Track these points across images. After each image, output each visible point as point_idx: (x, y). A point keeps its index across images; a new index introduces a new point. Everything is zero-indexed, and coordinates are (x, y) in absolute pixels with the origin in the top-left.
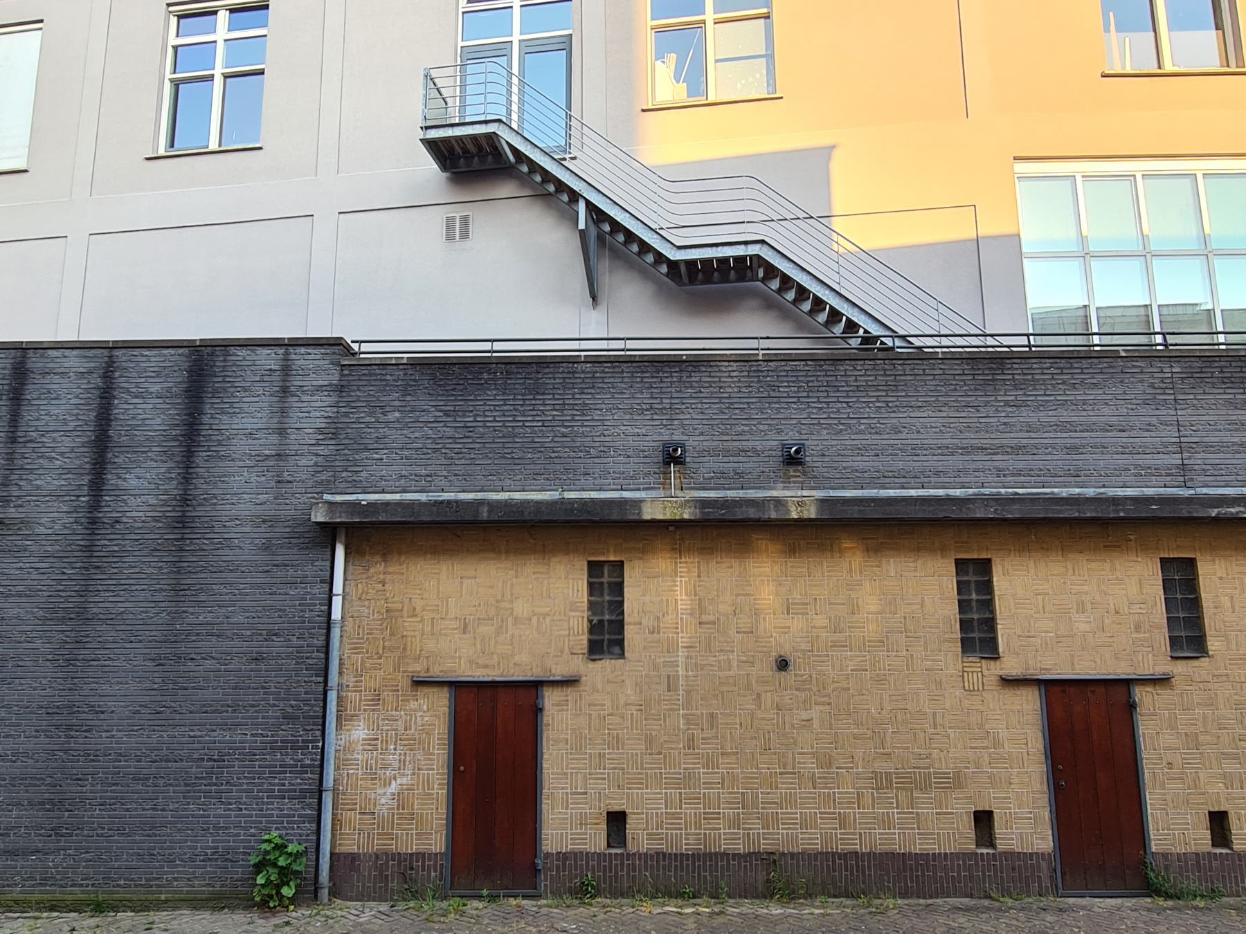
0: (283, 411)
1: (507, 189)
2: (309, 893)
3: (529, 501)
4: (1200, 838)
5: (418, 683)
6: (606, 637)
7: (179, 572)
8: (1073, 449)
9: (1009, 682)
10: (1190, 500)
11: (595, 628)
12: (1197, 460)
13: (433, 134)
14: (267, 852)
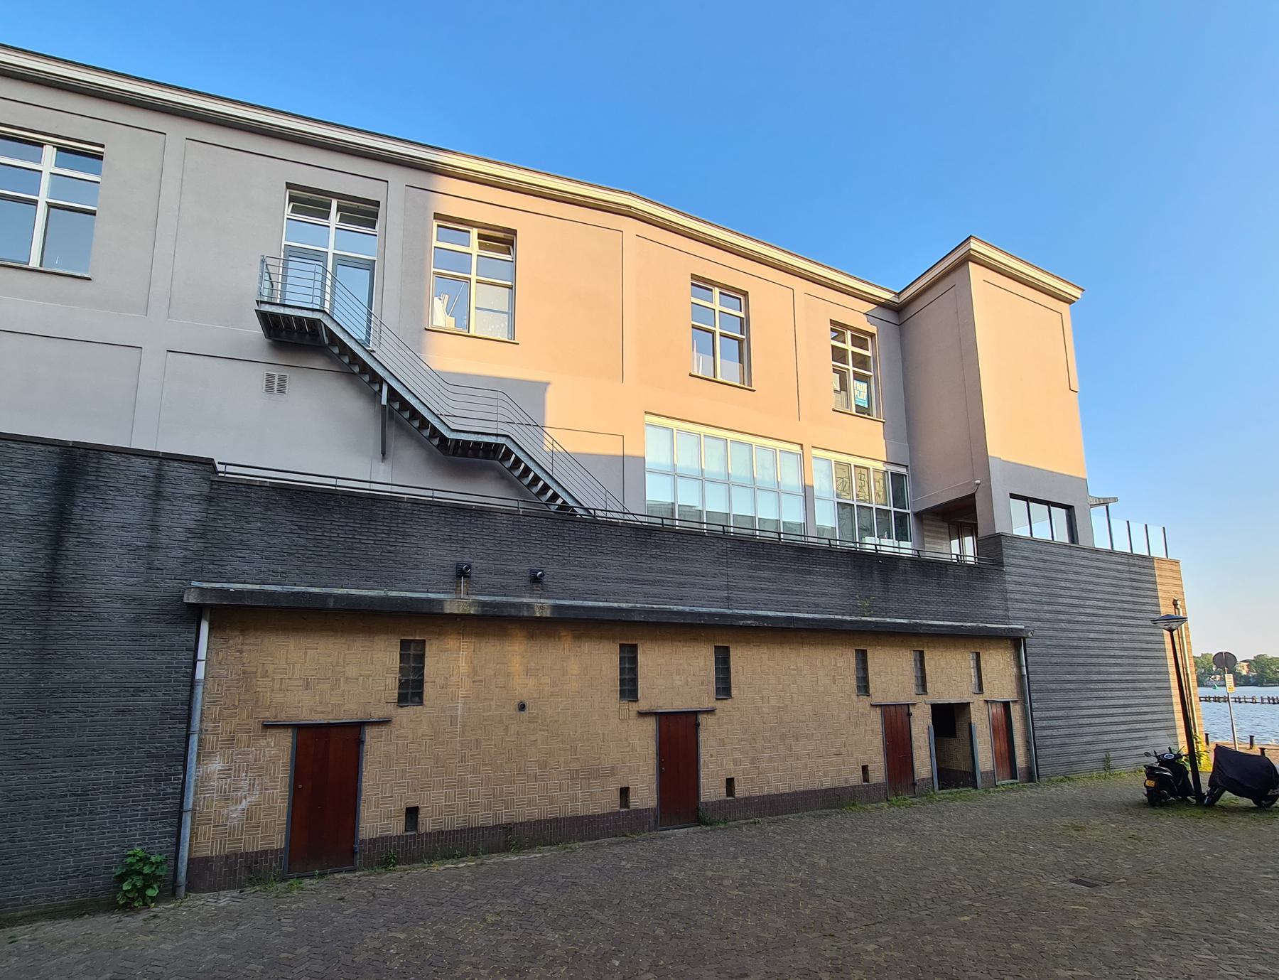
0: (156, 512)
1: (319, 363)
2: (170, 891)
3: (365, 596)
5: (267, 727)
6: (411, 690)
7: (44, 639)
8: (680, 585)
9: (642, 714)
10: (732, 616)
11: (402, 685)
12: (735, 594)
13: (267, 308)
14: (131, 864)
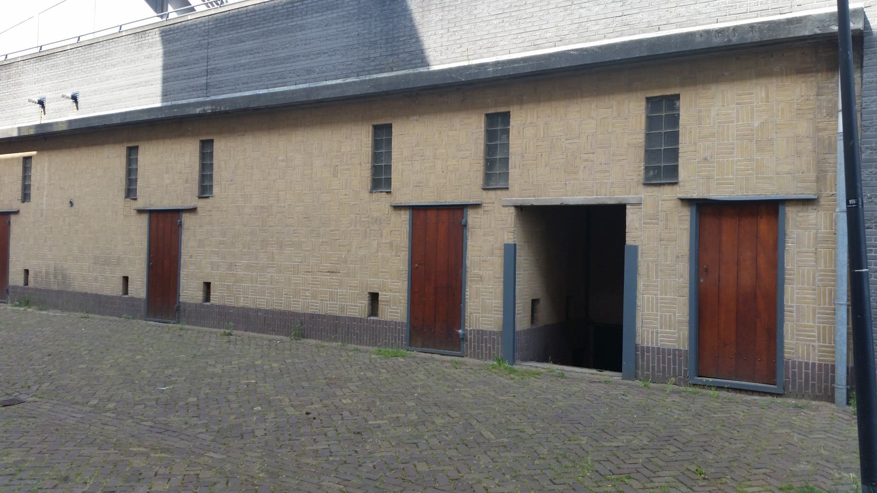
3: (237, 98)
4: (199, 295)
9: (397, 208)
